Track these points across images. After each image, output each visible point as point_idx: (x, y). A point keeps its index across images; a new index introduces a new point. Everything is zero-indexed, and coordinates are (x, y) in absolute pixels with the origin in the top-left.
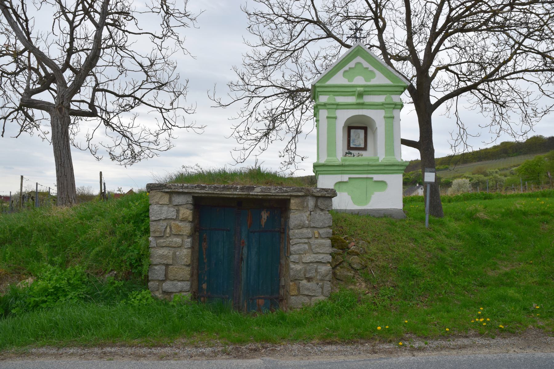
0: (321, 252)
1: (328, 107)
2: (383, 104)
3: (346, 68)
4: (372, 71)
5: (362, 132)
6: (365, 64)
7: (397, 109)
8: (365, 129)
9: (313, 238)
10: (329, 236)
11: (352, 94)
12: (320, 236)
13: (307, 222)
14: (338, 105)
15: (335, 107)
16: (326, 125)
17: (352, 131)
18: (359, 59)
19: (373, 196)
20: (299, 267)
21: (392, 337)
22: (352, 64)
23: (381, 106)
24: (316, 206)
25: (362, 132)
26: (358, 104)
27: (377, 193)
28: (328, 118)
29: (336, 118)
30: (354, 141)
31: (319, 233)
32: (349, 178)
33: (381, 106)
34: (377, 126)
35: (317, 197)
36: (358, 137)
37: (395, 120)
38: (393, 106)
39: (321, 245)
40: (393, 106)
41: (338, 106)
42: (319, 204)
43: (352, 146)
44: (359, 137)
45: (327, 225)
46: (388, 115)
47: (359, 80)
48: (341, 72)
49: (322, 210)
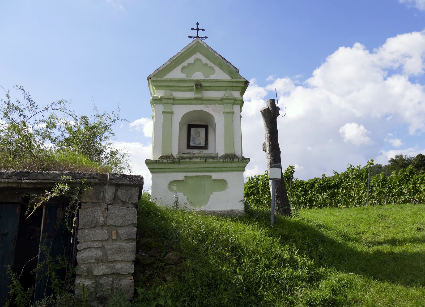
0: (120, 259)
1: (164, 101)
2: (222, 100)
3: (185, 64)
4: (211, 68)
5: (202, 131)
6: (205, 60)
7: (237, 104)
8: (206, 127)
9: (110, 240)
10: (131, 237)
11: (189, 89)
12: (119, 238)
13: (102, 219)
14: (174, 99)
15: (172, 101)
16: (162, 120)
17: (192, 129)
18: (198, 56)
19: (211, 196)
20: (87, 282)
21: (380, 275)
22: (191, 60)
23: (221, 101)
24: (115, 197)
25: (202, 131)
26: (196, 99)
27: (215, 193)
28: (163, 112)
29: (172, 113)
30: (193, 140)
31: (117, 233)
32: (185, 177)
33: (221, 101)
34: (216, 121)
35: (118, 186)
36: (198, 136)
37: (234, 115)
38: (233, 101)
39: (120, 250)
40: (233, 101)
41: (175, 101)
42: (119, 194)
43: (192, 144)
44: (199, 136)
45: (130, 222)
46: (228, 110)
47: (198, 76)
48: (179, 67)
49: (124, 203)
